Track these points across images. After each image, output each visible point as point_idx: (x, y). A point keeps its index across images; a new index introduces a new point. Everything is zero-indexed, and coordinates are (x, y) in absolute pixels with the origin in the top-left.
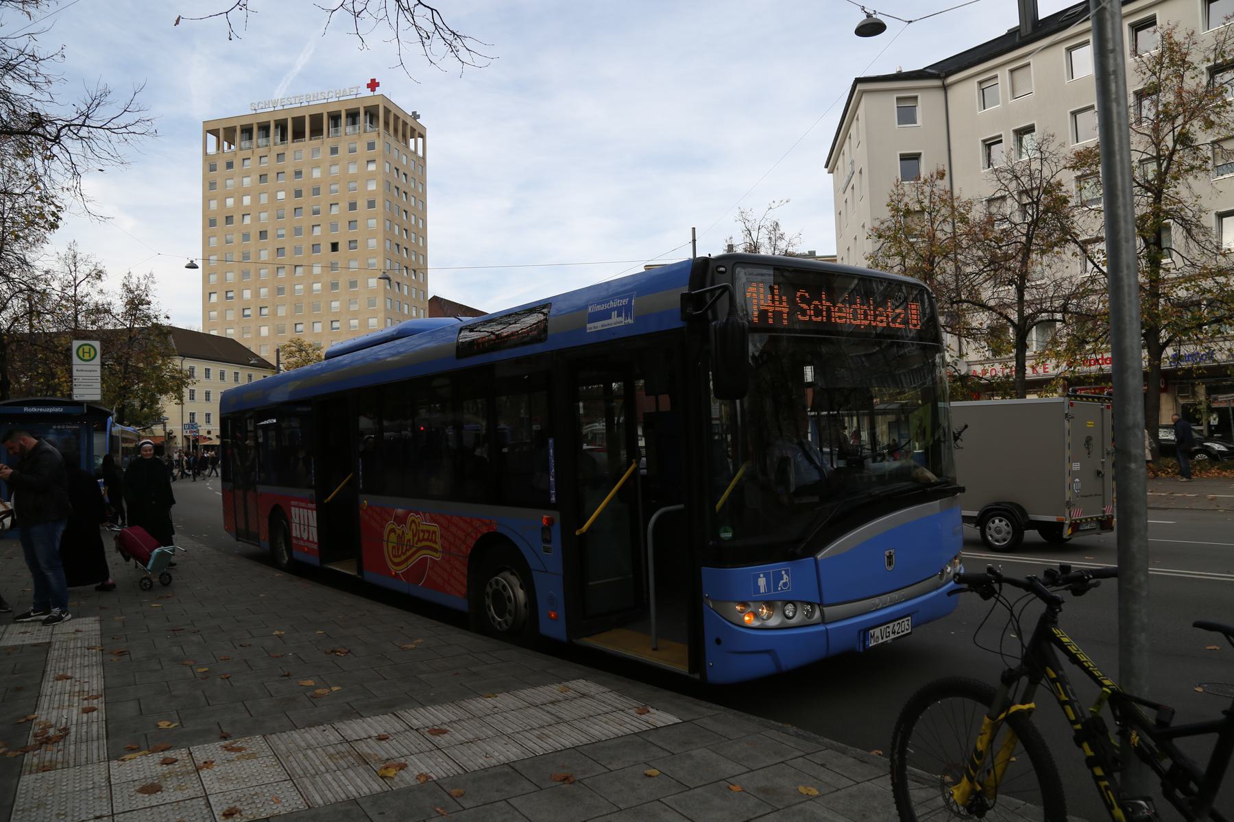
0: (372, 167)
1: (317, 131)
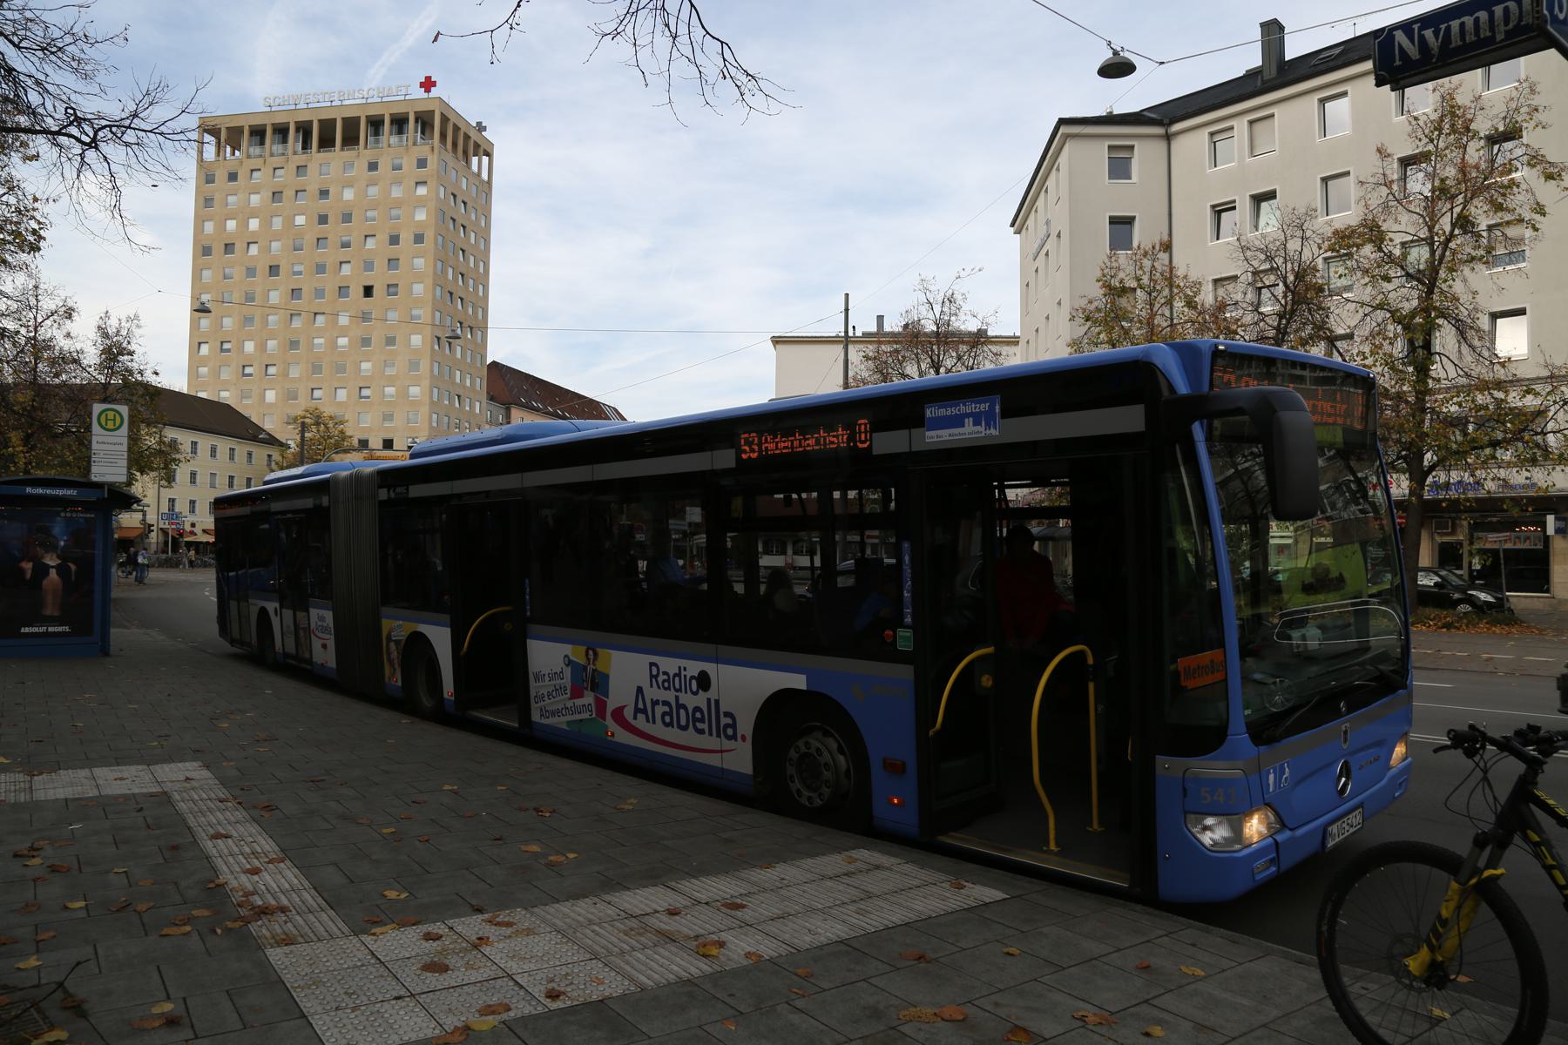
0: (422, 191)
1: (351, 139)
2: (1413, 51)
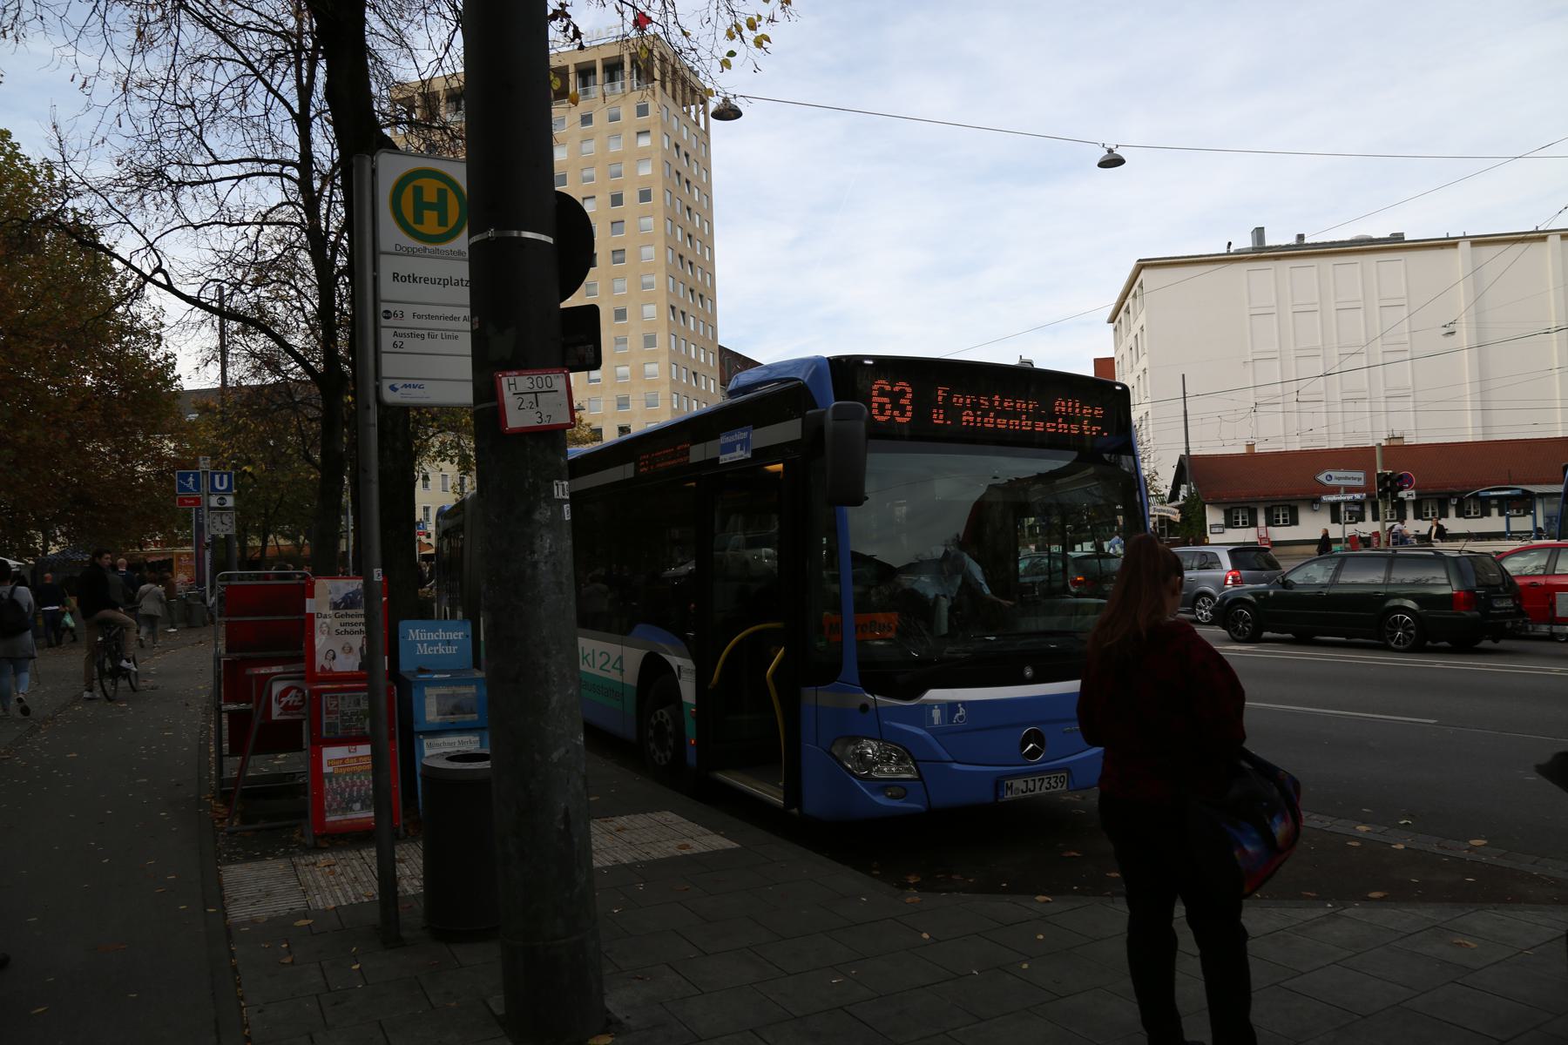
0: (644, 142)
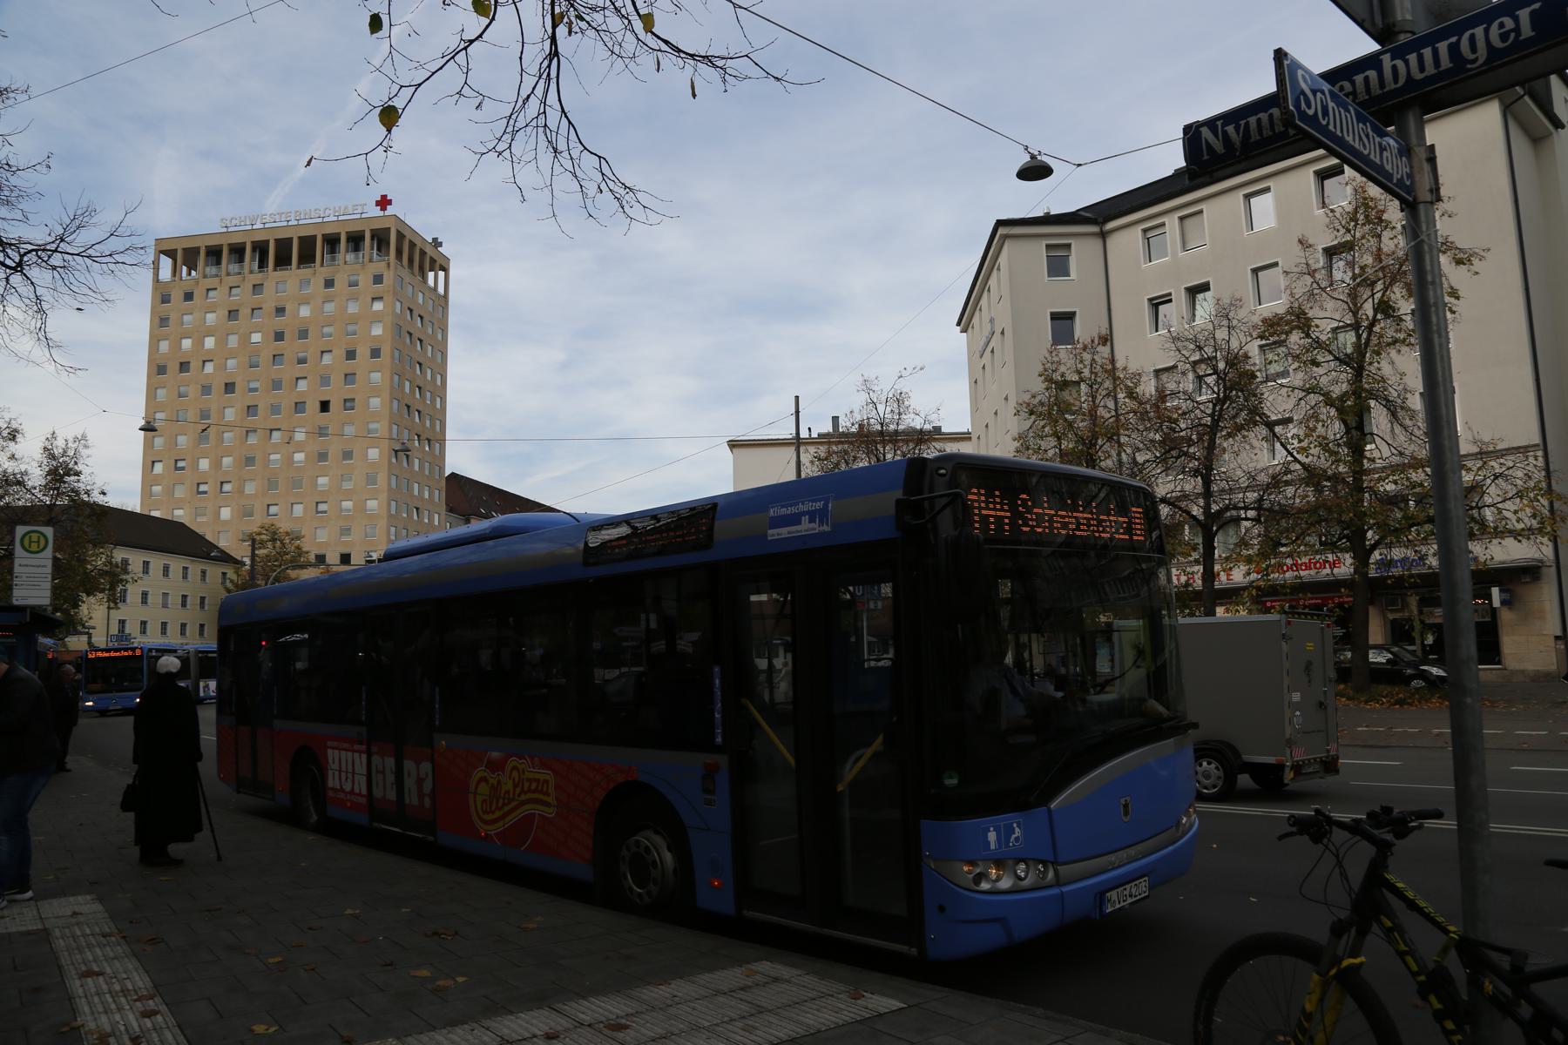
0: (378, 306)
1: (307, 258)
2: (1218, 146)
